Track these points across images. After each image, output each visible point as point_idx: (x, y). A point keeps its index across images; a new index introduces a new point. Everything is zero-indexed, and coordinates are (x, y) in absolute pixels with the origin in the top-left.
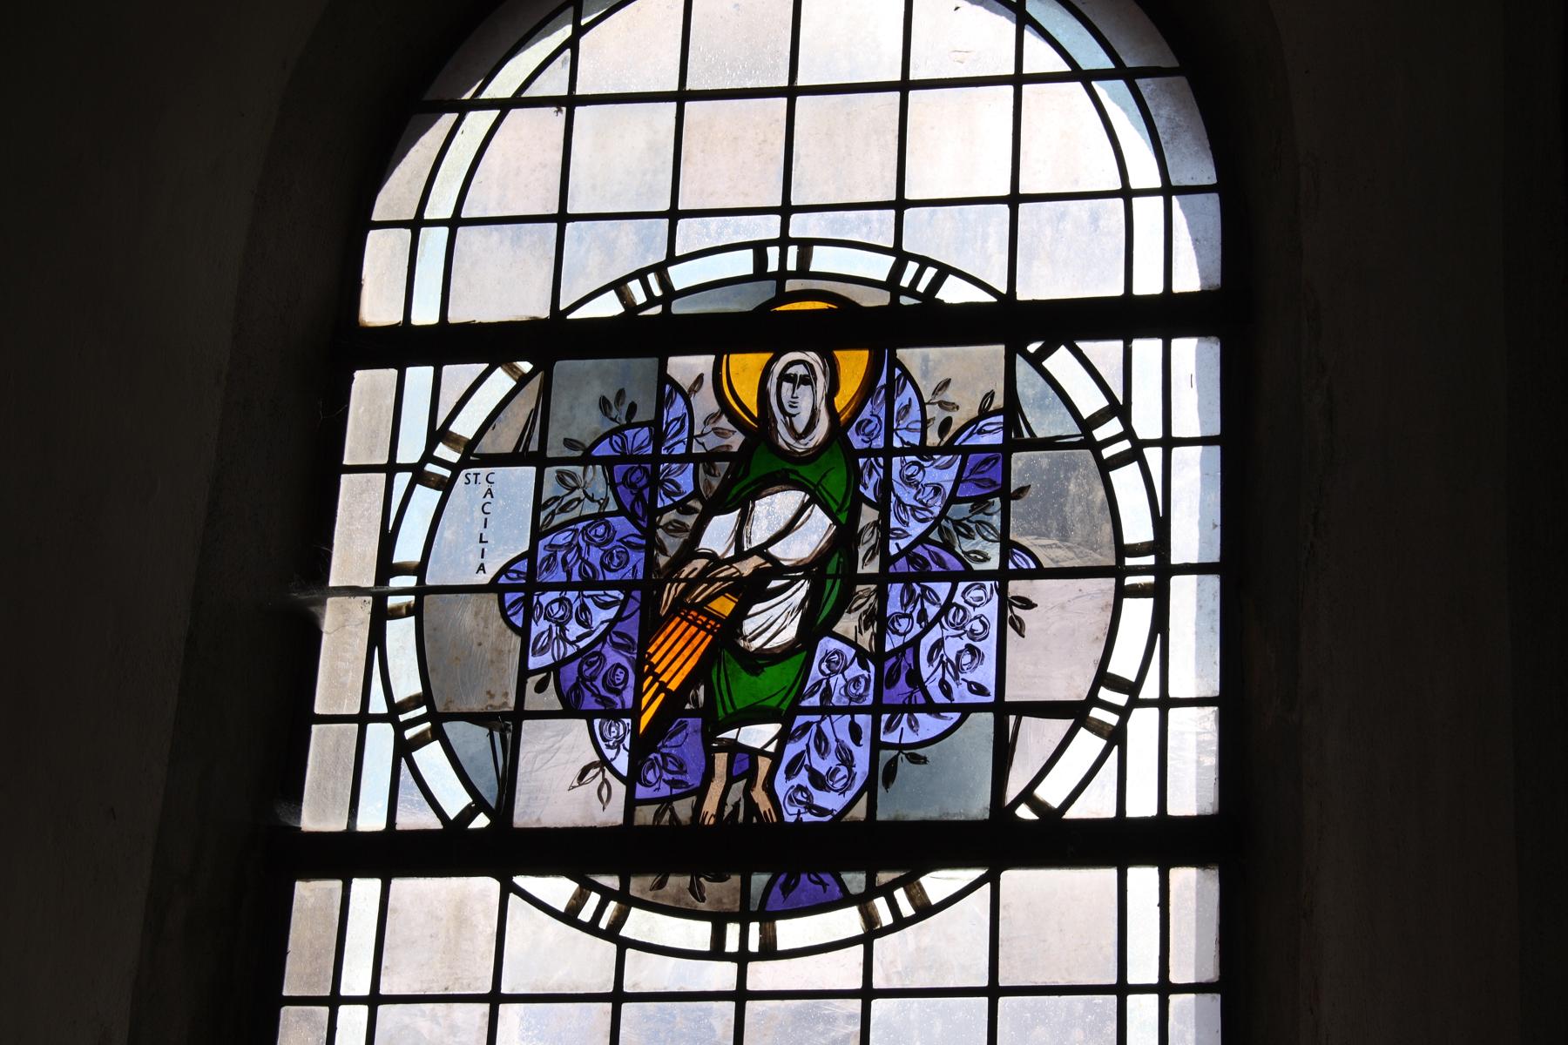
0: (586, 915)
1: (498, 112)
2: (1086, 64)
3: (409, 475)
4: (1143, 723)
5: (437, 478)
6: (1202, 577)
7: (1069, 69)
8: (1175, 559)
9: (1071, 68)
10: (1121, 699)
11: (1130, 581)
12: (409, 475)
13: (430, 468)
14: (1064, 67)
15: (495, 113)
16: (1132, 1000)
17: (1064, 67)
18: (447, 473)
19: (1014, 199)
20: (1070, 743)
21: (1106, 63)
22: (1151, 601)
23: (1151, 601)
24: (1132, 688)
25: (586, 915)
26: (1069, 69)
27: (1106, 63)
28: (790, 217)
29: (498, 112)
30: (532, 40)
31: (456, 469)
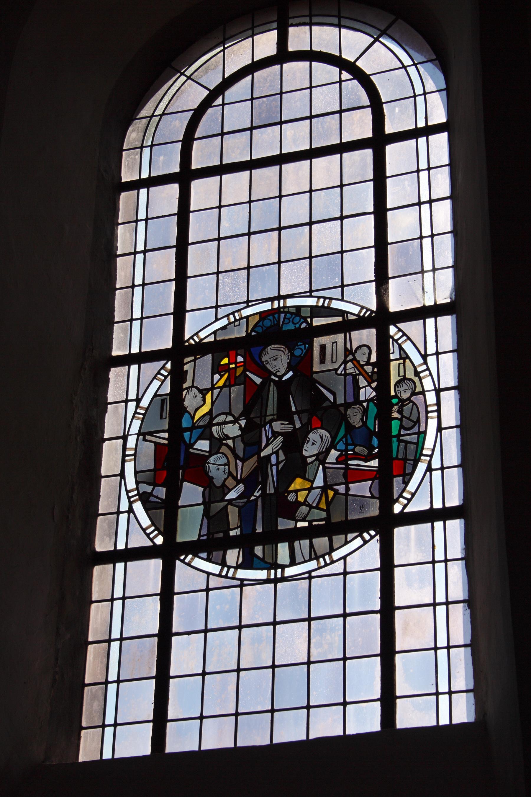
17: (222, 53)
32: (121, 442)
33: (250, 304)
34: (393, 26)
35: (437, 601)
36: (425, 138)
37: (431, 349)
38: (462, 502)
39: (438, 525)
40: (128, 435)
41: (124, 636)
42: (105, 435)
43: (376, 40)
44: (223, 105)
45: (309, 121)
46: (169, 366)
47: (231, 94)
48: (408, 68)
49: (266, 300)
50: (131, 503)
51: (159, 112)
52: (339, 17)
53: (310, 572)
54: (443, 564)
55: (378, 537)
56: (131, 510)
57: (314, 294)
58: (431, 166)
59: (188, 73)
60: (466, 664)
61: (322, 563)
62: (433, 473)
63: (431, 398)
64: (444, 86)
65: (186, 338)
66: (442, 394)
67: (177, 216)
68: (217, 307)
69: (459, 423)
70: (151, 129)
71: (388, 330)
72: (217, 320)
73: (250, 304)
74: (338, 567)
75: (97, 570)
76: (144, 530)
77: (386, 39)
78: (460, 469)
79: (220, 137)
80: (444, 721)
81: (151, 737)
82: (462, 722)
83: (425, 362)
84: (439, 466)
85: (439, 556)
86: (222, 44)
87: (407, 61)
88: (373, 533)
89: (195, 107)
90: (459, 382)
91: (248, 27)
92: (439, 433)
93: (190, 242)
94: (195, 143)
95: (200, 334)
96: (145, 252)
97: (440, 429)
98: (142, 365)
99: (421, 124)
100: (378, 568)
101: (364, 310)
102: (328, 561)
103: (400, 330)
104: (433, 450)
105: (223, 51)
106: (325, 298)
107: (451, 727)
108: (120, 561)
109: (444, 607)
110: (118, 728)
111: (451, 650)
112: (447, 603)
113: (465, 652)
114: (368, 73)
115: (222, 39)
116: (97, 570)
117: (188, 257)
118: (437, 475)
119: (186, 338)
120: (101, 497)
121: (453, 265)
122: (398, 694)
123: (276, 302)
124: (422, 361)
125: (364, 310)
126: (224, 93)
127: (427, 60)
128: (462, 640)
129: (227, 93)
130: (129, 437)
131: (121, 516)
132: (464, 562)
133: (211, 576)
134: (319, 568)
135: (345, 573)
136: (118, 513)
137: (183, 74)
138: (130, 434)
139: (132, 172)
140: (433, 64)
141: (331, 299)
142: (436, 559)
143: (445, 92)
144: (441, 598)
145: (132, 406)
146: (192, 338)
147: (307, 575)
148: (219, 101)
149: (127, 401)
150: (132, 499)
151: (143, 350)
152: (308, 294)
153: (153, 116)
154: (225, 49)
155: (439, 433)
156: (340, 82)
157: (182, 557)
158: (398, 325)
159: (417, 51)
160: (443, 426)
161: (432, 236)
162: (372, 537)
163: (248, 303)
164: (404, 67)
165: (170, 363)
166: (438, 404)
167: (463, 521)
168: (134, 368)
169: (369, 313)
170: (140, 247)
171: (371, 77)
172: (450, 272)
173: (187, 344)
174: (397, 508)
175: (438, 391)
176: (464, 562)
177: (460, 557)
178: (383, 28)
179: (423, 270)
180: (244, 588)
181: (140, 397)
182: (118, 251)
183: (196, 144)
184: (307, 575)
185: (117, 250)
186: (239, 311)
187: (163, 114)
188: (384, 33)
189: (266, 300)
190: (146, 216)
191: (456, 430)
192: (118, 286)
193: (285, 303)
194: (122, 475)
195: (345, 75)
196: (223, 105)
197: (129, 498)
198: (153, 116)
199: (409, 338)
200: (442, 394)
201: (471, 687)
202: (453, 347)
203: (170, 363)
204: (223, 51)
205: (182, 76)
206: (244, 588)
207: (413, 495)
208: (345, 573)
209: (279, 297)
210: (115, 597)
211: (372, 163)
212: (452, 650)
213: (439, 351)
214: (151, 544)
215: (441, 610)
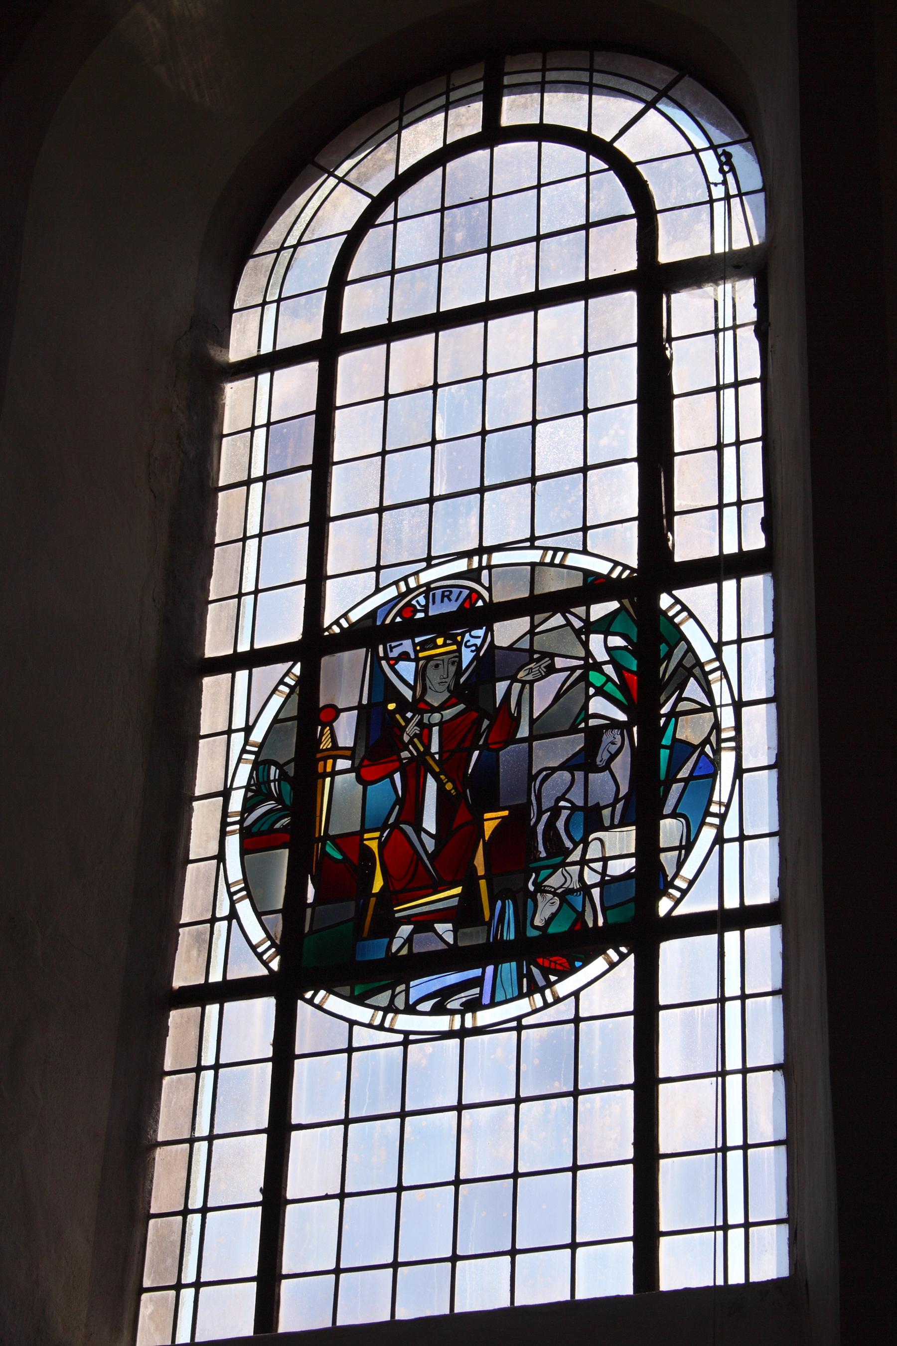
33: (434, 562)
34: (677, 86)
37: (730, 634)
38: (777, 895)
40: (232, 788)
41: (269, 471)
42: (211, 594)
43: (650, 105)
44: (395, 221)
45: (534, 244)
46: (297, 670)
47: (409, 201)
48: (701, 154)
49: (460, 555)
50: (233, 904)
51: (292, 240)
52: (591, 71)
53: (519, 1019)
55: (632, 956)
56: (233, 915)
57: (537, 543)
58: (750, 1142)
59: (340, 172)
61: (539, 1003)
62: (726, 845)
63: (727, 718)
65: (326, 625)
66: (744, 710)
67: (326, 291)
68: (378, 569)
69: (781, 1059)
70: (280, 269)
71: (657, 600)
72: (378, 590)
73: (434, 562)
74: (565, 1010)
75: (208, 682)
76: (254, 948)
78: (779, 1074)
79: (389, 277)
80: (736, 1277)
81: (304, 597)
83: (719, 658)
84: (741, 1221)
85: (730, 496)
87: (700, 142)
88: (623, 950)
89: (349, 228)
91: (441, 92)
92: (737, 781)
93: (332, 515)
94: (347, 289)
95: (350, 615)
97: (739, 772)
98: (254, 670)
100: (632, 854)
101: (619, 569)
102: (550, 999)
103: (677, 601)
104: (728, 806)
106: (556, 550)
107: (748, 1286)
108: (212, 1002)
109: (740, 1076)
110: (203, 1290)
111: (750, 1151)
114: (633, 160)
116: (208, 682)
117: (291, 1113)
118: (731, 850)
119: (326, 625)
122: (662, 1001)
123: (476, 559)
124: (714, 656)
125: (619, 569)
126: (398, 200)
127: (732, 141)
128: (767, 762)
129: (401, 199)
130: (234, 793)
131: (217, 925)
133: (356, 1028)
134: (535, 1011)
135: (577, 1020)
136: (213, 920)
137: (331, 174)
138: (234, 787)
139: (198, 932)
140: (744, 147)
141: (567, 551)
145: (238, 739)
146: (337, 622)
147: (514, 1024)
148: (388, 215)
149: (229, 732)
150: (235, 897)
152: (528, 544)
153: (282, 248)
155: (737, 781)
156: (588, 174)
158: (674, 592)
159: (717, 127)
160: (744, 766)
162: (623, 957)
163: (429, 561)
164: (695, 151)
165: (299, 665)
166: (738, 728)
168: (242, 676)
169: (627, 572)
170: (253, 529)
171: (638, 167)
173: (326, 633)
174: (664, 906)
175: (738, 705)
178: (661, 87)
179: (717, 336)
180: (411, 1047)
181: (251, 723)
182: (217, 538)
183: (349, 291)
184: (514, 1024)
185: (209, 596)
186: (416, 574)
187: (300, 243)
188: (663, 94)
189: (460, 555)
190: (246, 721)
191: (773, 1001)
192: (217, 541)
193: (489, 559)
194: (221, 857)
195: (597, 164)
196: (395, 221)
197: (231, 895)
198: (282, 248)
199: (691, 615)
200: (744, 710)
201: (782, 1136)
202: (765, 630)
203: (299, 665)
205: (331, 178)
206: (410, 1047)
207: (691, 883)
208: (577, 1020)
209: (462, 1034)
210: (233, 727)
212: (750, 1151)
213: (743, 499)
214: (265, 972)
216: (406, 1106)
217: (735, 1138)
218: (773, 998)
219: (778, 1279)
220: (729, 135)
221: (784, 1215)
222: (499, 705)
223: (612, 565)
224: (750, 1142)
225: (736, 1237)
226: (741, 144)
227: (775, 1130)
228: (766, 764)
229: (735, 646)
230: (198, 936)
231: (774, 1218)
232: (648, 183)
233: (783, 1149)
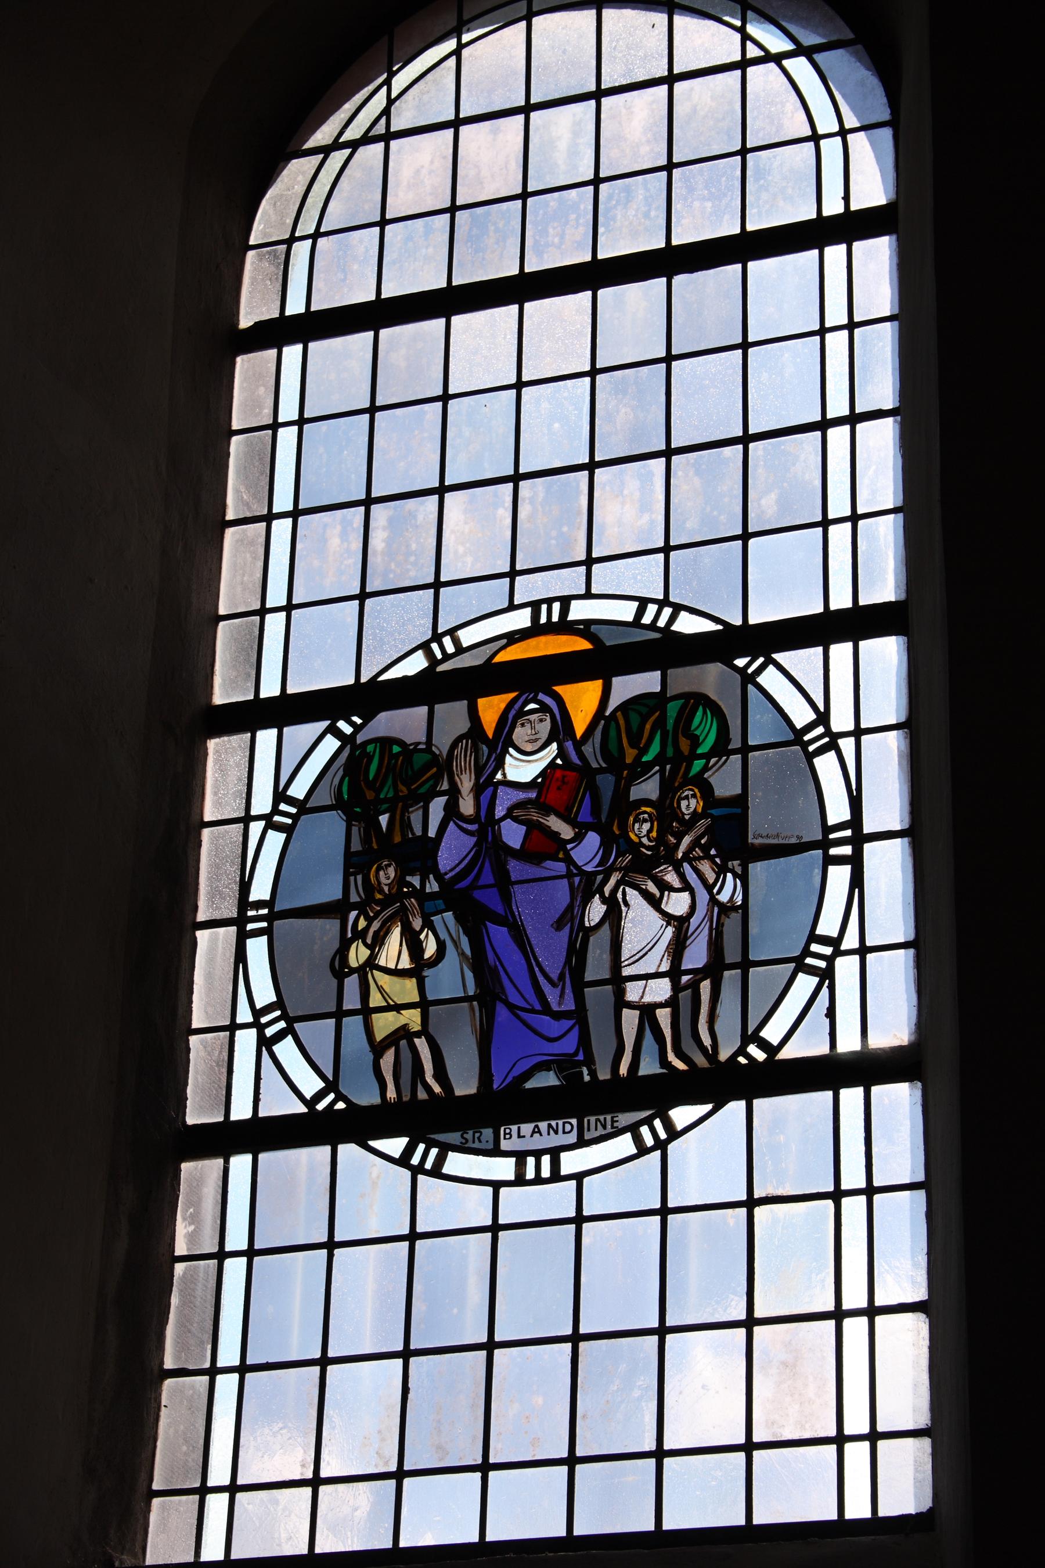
0: (530, 1174)
1: (351, 150)
2: (774, 50)
3: (262, 823)
4: (846, 968)
5: (300, 802)
6: (906, 950)
7: (392, 98)
8: (867, 829)
9: (854, 34)
10: (828, 951)
11: (833, 851)
12: (262, 823)
13: (277, 818)
14: (453, 60)
15: (348, 151)
16: (865, 1429)
17: (453, 60)
18: (289, 821)
19: (664, 1211)
20: (800, 1014)
21: (788, 46)
22: (849, 867)
23: (849, 867)
24: (834, 942)
25: (530, 1174)
26: (392, 98)
27: (788, 46)
28: (365, 601)
29: (351, 150)
30: (450, 37)
31: (295, 817)
32: (234, 929)
35: (846, 1306)
36: (843, 247)
38: (892, 196)
39: (852, 1097)
54: (863, 1198)
60: (913, 1126)
64: (885, 115)
77: (758, 25)
80: (858, 1509)
82: (905, 1512)
86: (455, 34)
90: (908, 591)
96: (295, 514)
99: (833, 207)
105: (457, 53)
107: (876, 1525)
112: (870, 1191)
113: (890, 241)
115: (454, 23)
120: (191, 1051)
121: (898, 405)
128: (908, 1173)
132: (911, 952)
142: (848, 1431)
143: (887, 133)
144: (855, 1297)
151: (291, 690)
154: (461, 46)
157: (341, 1105)
161: (851, 326)
167: (894, 237)
172: (903, 958)
176: (911, 952)
177: (897, 827)
204: (457, 53)
211: (702, 547)
215: (855, 1328)
216: (520, 468)
217: (853, 1177)
218: (890, 238)
219: (910, 1183)
220: (823, 36)
221: (920, 1177)
222: (424, 930)
223: (635, 604)
224: (869, 943)
225: (854, 1208)
226: (850, 49)
227: (913, 1172)
228: (902, 940)
229: (848, 525)
230: (250, 453)
231: (907, 1181)
232: (493, 1078)
233: (921, 1195)
